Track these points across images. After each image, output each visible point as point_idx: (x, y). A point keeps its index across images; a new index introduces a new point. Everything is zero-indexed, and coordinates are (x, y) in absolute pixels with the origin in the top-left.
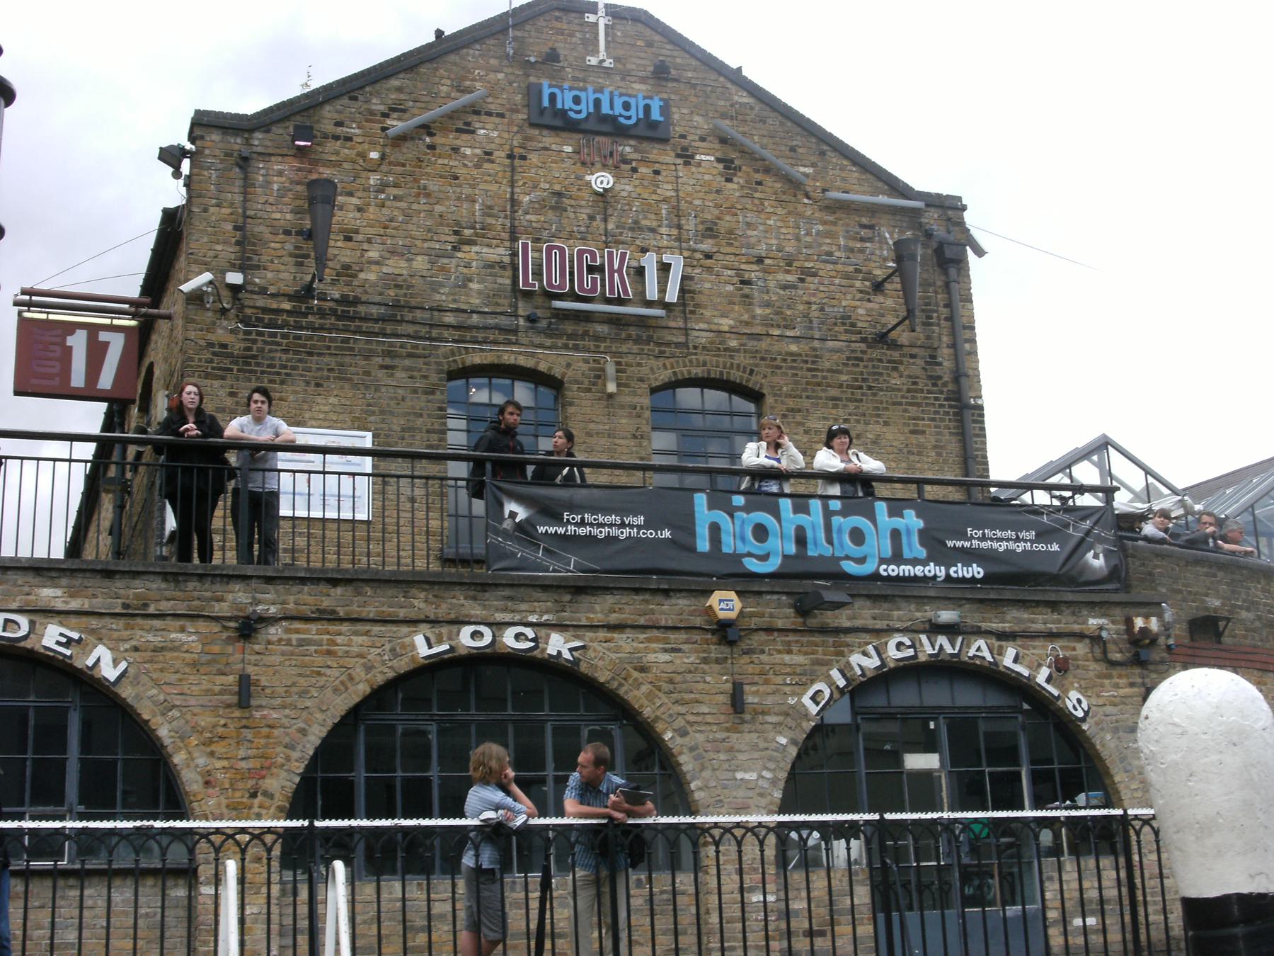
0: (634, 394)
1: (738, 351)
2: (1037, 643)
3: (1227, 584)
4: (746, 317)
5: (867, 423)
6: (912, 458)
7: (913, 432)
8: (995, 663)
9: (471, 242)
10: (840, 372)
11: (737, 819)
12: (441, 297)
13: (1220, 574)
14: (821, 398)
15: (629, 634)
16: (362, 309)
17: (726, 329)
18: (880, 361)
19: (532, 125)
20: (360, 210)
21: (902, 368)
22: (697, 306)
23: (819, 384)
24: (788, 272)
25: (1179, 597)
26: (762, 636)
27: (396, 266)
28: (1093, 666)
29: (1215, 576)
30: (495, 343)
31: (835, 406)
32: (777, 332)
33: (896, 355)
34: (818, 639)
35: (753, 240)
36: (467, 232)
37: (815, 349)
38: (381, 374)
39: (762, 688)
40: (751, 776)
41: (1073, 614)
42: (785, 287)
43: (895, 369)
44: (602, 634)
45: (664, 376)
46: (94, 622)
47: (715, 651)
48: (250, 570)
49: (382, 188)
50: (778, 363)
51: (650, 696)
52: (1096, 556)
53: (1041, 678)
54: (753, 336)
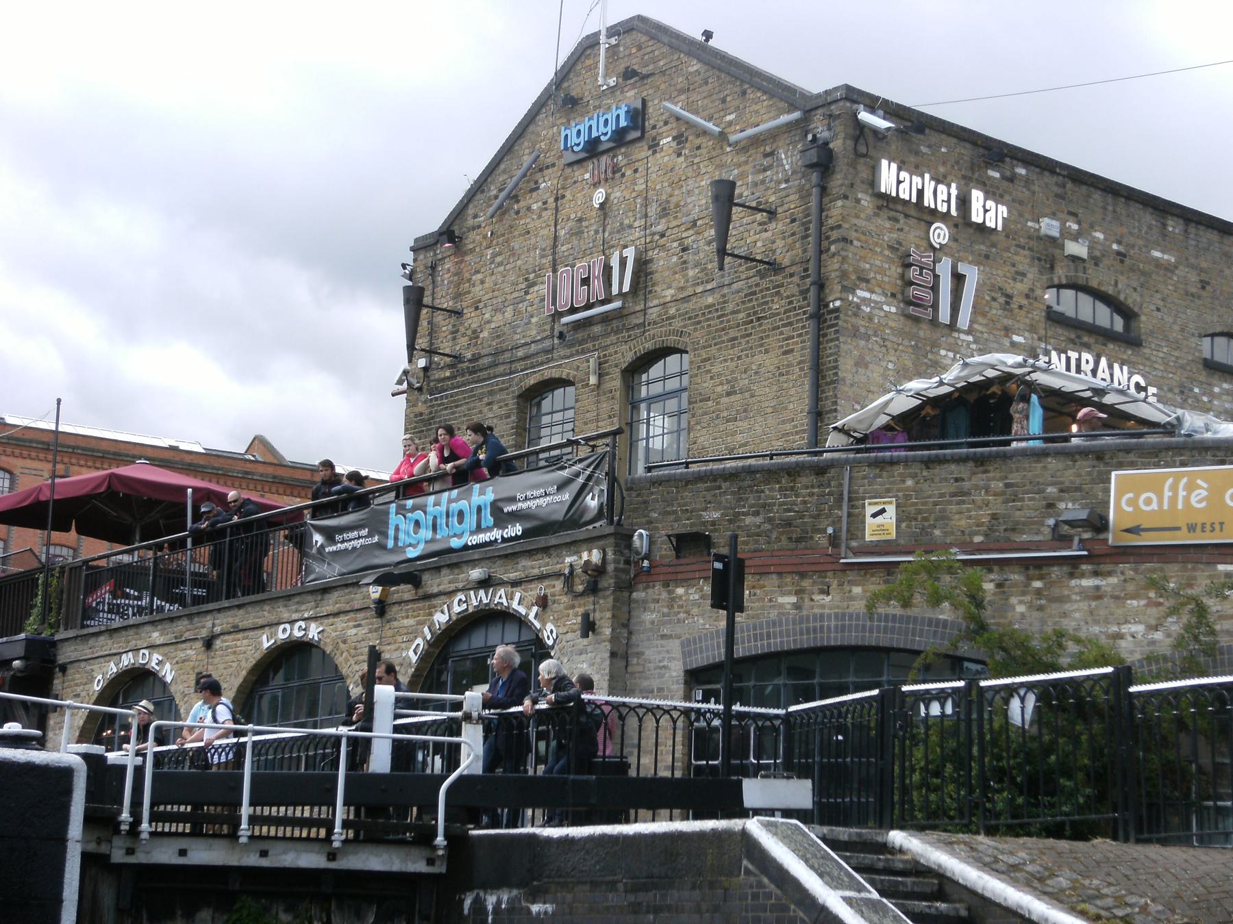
1: (673, 317)
3: (733, 493)
4: (682, 284)
6: (782, 379)
7: (785, 353)
10: (738, 312)
11: (658, 702)
12: (519, 339)
13: (725, 485)
14: (723, 342)
15: (344, 618)
16: (481, 362)
17: (669, 299)
18: (768, 289)
21: (782, 290)
22: (654, 285)
23: (723, 329)
25: (672, 517)
28: (564, 599)
29: (720, 487)
30: (542, 364)
32: (699, 289)
33: (779, 278)
36: (532, 276)
37: (724, 296)
38: (485, 410)
41: (286, 606)
43: (778, 293)
44: (331, 620)
45: (629, 357)
46: (166, 649)
47: (377, 622)
48: (187, 611)
49: (494, 256)
51: (347, 660)
52: (593, 499)
53: (531, 617)
54: (686, 299)
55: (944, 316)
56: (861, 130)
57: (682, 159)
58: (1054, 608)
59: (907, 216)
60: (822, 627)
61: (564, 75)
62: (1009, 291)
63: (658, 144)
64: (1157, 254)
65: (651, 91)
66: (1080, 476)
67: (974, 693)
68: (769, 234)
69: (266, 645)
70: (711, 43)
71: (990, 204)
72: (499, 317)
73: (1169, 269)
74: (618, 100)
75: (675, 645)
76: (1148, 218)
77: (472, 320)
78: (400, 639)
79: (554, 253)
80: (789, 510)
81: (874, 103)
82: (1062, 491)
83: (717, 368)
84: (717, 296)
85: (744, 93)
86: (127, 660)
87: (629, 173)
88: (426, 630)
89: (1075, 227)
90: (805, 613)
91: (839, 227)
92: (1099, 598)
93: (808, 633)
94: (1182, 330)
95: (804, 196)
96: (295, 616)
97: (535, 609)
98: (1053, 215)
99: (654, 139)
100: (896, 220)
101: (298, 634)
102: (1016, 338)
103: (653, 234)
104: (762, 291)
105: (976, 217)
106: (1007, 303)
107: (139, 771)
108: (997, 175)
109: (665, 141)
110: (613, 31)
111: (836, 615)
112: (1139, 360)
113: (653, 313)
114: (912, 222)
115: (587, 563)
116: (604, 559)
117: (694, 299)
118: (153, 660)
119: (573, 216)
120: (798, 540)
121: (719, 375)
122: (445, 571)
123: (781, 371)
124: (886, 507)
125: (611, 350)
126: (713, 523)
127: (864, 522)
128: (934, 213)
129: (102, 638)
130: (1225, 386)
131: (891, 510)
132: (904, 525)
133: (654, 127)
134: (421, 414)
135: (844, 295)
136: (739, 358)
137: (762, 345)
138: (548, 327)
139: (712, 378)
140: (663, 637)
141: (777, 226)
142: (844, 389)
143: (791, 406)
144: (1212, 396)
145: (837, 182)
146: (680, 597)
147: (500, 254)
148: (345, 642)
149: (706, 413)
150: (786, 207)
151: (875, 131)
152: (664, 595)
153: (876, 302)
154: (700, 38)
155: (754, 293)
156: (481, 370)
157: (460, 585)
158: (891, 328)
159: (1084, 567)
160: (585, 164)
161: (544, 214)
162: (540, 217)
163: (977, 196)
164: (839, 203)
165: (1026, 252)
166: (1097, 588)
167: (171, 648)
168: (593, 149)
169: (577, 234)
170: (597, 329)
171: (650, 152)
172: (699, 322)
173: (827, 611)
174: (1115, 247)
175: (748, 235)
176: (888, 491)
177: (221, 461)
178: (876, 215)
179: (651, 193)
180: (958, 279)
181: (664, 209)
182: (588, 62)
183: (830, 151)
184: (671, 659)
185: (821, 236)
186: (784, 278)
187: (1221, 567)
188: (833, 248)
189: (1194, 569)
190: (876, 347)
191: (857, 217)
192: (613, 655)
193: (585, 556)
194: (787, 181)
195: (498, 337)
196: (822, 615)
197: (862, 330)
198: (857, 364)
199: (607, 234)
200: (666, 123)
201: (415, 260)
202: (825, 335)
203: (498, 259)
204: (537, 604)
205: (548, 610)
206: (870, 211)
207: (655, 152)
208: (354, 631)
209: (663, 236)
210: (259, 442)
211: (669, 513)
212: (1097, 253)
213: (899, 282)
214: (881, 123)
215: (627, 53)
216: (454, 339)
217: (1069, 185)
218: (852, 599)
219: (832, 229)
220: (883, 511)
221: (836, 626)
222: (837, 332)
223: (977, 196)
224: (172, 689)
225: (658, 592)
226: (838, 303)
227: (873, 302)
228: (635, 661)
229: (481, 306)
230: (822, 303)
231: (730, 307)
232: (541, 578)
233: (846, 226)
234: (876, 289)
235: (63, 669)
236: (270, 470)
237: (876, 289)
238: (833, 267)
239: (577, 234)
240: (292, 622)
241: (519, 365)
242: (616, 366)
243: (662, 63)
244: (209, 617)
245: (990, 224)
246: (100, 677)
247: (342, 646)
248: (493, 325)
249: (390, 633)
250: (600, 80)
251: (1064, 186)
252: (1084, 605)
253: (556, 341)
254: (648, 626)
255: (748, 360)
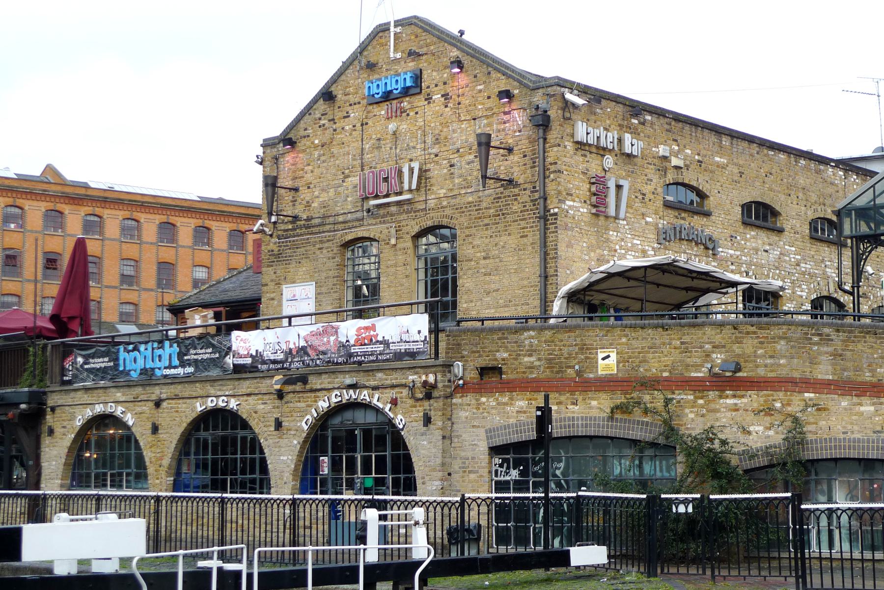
0: (405, 241)
1: (446, 207)
2: (387, 391)
4: (451, 187)
5: (500, 236)
7: (521, 237)
8: (370, 402)
9: (348, 176)
10: (490, 208)
12: (339, 210)
15: (253, 397)
17: (442, 195)
18: (509, 196)
19: (370, 104)
20: (312, 172)
21: (519, 198)
22: (431, 185)
23: (480, 218)
24: (470, 154)
25: (477, 355)
26: (291, 395)
27: (324, 197)
30: (356, 227)
31: (487, 229)
32: (463, 191)
33: (516, 190)
34: (309, 395)
35: (455, 140)
36: (347, 171)
37: (479, 197)
38: (318, 252)
39: (290, 419)
40: (285, 458)
41: (211, 386)
42: (469, 163)
43: (516, 199)
44: (245, 398)
45: (416, 229)
46: (127, 404)
47: (277, 402)
49: (320, 156)
50: (464, 209)
51: (257, 424)
53: (387, 410)
54: (454, 197)
55: (612, 211)
56: (567, 105)
57: (448, 109)
58: (711, 416)
59: (591, 153)
60: (573, 425)
61: (363, 47)
62: (644, 192)
63: (431, 98)
64: (717, 159)
65: (425, 64)
66: (724, 339)
67: (706, 502)
68: (508, 163)
69: (199, 409)
70: (463, 37)
71: (635, 141)
72: (324, 195)
73: (723, 167)
74: (402, 67)
75: (482, 433)
76: (713, 138)
77: (305, 195)
78: (295, 414)
79: (362, 159)
80: (551, 354)
81: (572, 86)
82: (714, 347)
83: (477, 242)
84: (475, 197)
85: (489, 73)
86: (99, 409)
87: (412, 114)
88: (313, 411)
89: (676, 148)
90: (563, 416)
91: (556, 163)
92: (737, 410)
93: (565, 428)
94: (731, 203)
95: (532, 142)
96: (219, 393)
97: (389, 406)
98: (665, 143)
99: (428, 95)
100: (585, 156)
101: (221, 404)
102: (648, 219)
103: (430, 154)
104: (505, 197)
105: (628, 150)
106: (643, 199)
107: (250, 576)
108: (636, 122)
109: (436, 97)
110: (398, 23)
111: (582, 418)
112: (710, 224)
113: (432, 203)
114: (593, 156)
115: (425, 382)
116: (436, 379)
117: (459, 197)
118: (119, 411)
119: (374, 137)
120: (558, 372)
121: (478, 246)
122: (324, 376)
123: (519, 249)
124: (611, 354)
125: (404, 223)
126: (503, 360)
127: (597, 363)
128: (604, 149)
129: (79, 393)
130: (753, 233)
131: (614, 356)
132: (621, 365)
133: (428, 87)
134: (272, 251)
135: (559, 205)
136: (491, 237)
137: (506, 230)
138: (359, 204)
139: (473, 247)
140: (473, 426)
141: (515, 158)
142: (561, 262)
143: (527, 270)
144: (746, 240)
145: (553, 136)
146: (484, 403)
147: (324, 155)
148: (256, 412)
149: (470, 269)
150: (520, 147)
151: (573, 104)
152: (474, 402)
153: (576, 207)
154: (456, 32)
155: (500, 198)
156: (313, 227)
157: (337, 386)
158: (585, 222)
159: (728, 392)
160: (381, 104)
161: (354, 133)
162: (351, 134)
163: (628, 137)
164: (555, 149)
165: (652, 167)
166: (736, 404)
167: (131, 404)
168: (387, 97)
169: (377, 148)
170: (393, 209)
171: (426, 102)
172: (463, 212)
173: (575, 415)
174: (697, 157)
175: (498, 164)
176: (611, 344)
177: (28, 183)
178: (575, 154)
179: (427, 128)
180: (619, 187)
181: (437, 139)
182: (383, 40)
183: (549, 117)
184: (479, 440)
185: (544, 171)
186: (520, 190)
187: (806, 395)
188: (552, 176)
189: (791, 395)
190: (577, 234)
191: (565, 156)
192: (444, 437)
193: (424, 378)
194: (520, 131)
195: (324, 207)
196: (573, 418)
197: (570, 225)
198: (567, 246)
199: (398, 151)
200: (436, 86)
201: (264, 153)
202: (548, 229)
203: (323, 158)
204: (390, 403)
205: (398, 406)
206: (572, 152)
207: (429, 103)
208: (262, 406)
209: (436, 156)
210: (50, 169)
211: (474, 352)
212: (688, 163)
213: (588, 193)
214: (579, 101)
215: (408, 38)
216: (294, 205)
217: (673, 123)
218: (591, 408)
219: (551, 164)
220: (608, 357)
221: (582, 425)
222: (556, 227)
223: (628, 137)
224: (134, 430)
225: (470, 398)
226: (556, 210)
227: (576, 208)
228: (456, 440)
229: (312, 186)
230: (546, 210)
231: (484, 205)
232: (393, 386)
233: (559, 163)
234: (577, 199)
235: (53, 409)
236: (59, 188)
237: (577, 199)
238: (551, 188)
239: (377, 148)
240: (217, 397)
241: (340, 227)
242: (408, 233)
243: (432, 48)
244: (157, 388)
245: (635, 153)
246: (80, 417)
247: (254, 415)
248: (321, 200)
249: (287, 410)
250: (392, 55)
251: (670, 124)
252: (729, 414)
253: (365, 214)
254: (464, 420)
255: (497, 239)
